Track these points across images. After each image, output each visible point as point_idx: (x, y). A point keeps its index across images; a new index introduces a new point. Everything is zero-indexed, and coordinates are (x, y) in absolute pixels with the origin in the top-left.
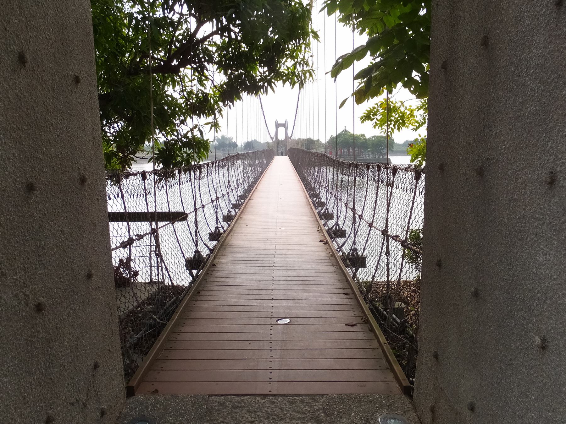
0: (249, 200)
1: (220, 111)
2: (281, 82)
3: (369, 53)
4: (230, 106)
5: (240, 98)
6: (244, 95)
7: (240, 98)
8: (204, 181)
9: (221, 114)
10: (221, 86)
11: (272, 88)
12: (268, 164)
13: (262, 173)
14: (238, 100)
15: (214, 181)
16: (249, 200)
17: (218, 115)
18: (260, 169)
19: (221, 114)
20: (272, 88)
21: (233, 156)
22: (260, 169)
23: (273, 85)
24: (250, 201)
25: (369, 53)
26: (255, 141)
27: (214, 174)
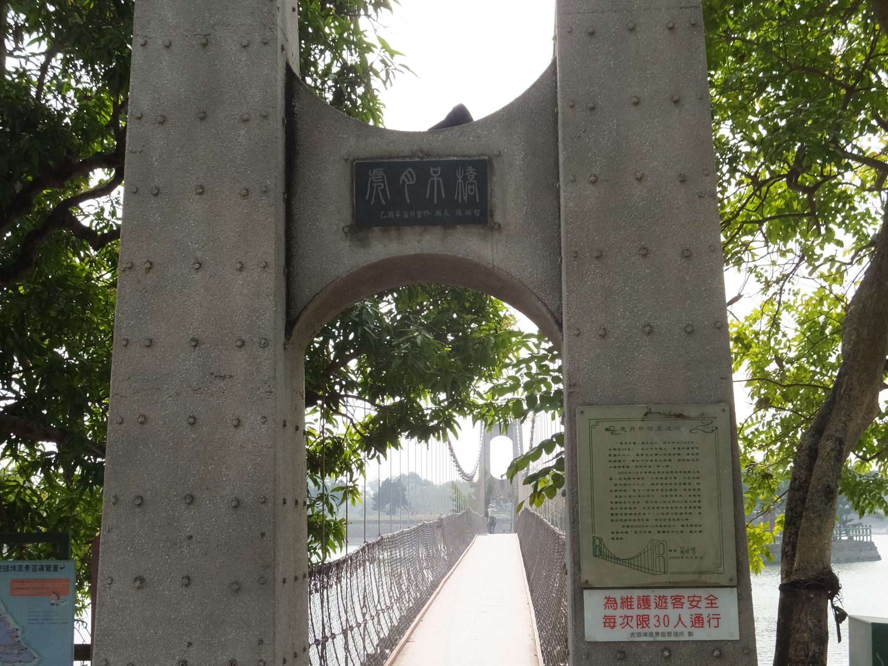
0: (407, 641)
1: (361, 467)
2: (470, 418)
3: (544, 452)
4: (378, 458)
5: (396, 445)
6: (403, 439)
7: (396, 445)
8: (333, 591)
9: (363, 472)
10: (365, 426)
11: (452, 429)
12: (450, 564)
13: (434, 585)
14: (393, 448)
15: (344, 593)
16: (407, 641)
17: (356, 474)
18: (429, 576)
19: (363, 472)
20: (452, 429)
21: (374, 545)
22: (429, 576)
23: (455, 426)
24: (408, 645)
25: (544, 452)
26: (414, 476)
27: (344, 581)
